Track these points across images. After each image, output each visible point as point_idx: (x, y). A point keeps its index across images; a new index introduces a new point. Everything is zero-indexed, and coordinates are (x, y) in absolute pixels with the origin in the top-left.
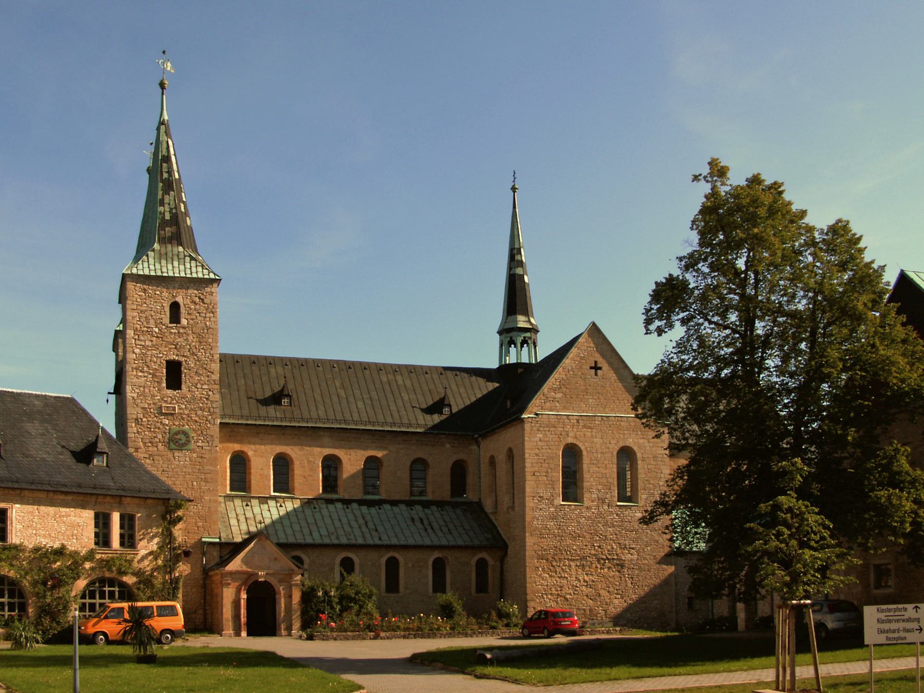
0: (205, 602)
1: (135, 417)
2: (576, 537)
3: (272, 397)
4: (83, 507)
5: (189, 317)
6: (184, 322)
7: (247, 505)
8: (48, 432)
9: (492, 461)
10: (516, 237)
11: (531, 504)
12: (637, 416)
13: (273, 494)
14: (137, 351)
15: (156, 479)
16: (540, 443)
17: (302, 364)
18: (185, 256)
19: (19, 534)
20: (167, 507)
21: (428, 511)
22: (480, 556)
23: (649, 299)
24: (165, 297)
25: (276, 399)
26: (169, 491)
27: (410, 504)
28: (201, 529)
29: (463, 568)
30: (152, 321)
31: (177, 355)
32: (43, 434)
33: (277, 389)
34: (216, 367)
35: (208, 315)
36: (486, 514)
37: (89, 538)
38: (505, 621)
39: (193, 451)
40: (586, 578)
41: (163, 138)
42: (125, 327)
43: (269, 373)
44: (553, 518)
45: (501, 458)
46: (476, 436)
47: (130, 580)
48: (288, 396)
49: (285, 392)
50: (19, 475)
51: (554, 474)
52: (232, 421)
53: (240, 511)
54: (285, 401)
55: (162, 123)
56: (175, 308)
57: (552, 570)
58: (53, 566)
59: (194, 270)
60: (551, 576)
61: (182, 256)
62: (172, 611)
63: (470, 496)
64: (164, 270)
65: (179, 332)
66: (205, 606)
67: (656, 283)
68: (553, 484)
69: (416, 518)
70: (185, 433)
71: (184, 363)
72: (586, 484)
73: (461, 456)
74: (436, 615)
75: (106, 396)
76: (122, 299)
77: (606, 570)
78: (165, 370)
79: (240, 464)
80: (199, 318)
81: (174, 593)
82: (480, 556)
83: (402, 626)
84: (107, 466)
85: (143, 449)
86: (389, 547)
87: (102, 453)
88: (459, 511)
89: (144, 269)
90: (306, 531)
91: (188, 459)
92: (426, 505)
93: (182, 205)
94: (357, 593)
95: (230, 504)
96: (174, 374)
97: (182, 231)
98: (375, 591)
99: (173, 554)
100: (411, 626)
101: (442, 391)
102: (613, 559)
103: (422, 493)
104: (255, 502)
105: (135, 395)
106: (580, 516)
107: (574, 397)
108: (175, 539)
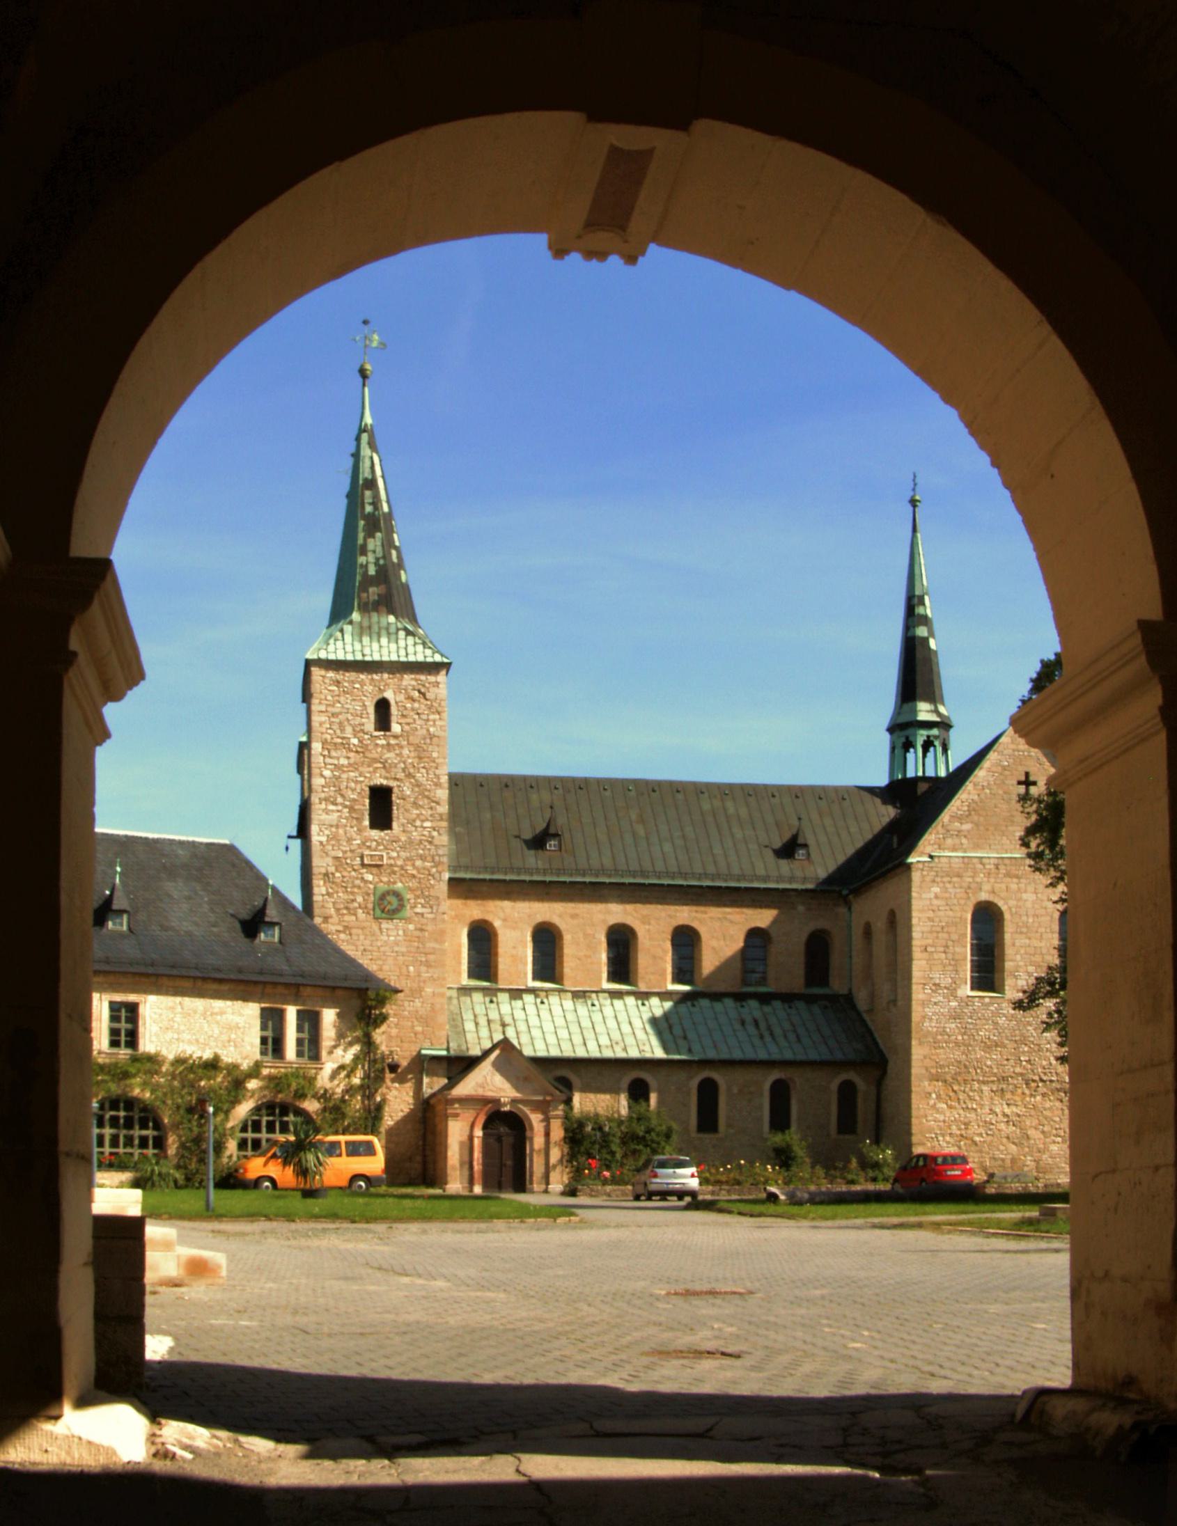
0: (424, 1145)
1: (323, 871)
2: (989, 1046)
3: (535, 842)
4: (245, 998)
5: (403, 721)
6: (396, 728)
7: (491, 1002)
8: (196, 894)
9: (868, 932)
10: (917, 578)
11: (921, 996)
12: (1029, 855)
13: (532, 984)
14: (327, 773)
15: (352, 961)
16: (935, 902)
17: (581, 786)
18: (398, 630)
19: (154, 1039)
20: (365, 1001)
21: (767, 1009)
22: (844, 1076)
23: (1029, 686)
24: (368, 688)
25: (538, 842)
26: (368, 976)
27: (740, 997)
28: (420, 1036)
29: (815, 1097)
30: (349, 730)
31: (386, 778)
32: (189, 898)
33: (541, 826)
34: (443, 794)
35: (432, 717)
36: (859, 1014)
37: (252, 1045)
38: (871, 1174)
39: (408, 920)
40: (1007, 1110)
41: (366, 451)
42: (309, 737)
43: (528, 802)
44: (955, 1016)
45: (880, 925)
46: (845, 892)
47: (311, 1106)
48: (556, 835)
49: (552, 831)
50: (154, 956)
51: (957, 949)
52: (468, 876)
53: (480, 1010)
54: (552, 844)
55: (362, 430)
56: (383, 708)
57: (952, 1097)
58: (204, 1083)
59: (411, 649)
60: (950, 1107)
61: (393, 629)
62: (369, 1150)
63: (837, 985)
64: (367, 651)
65: (388, 744)
66: (424, 1150)
67: (1042, 661)
68: (956, 964)
69: (748, 1019)
70: (397, 894)
71: (395, 790)
72: (1008, 965)
73: (821, 924)
74: (764, 1165)
75: (285, 841)
76: (307, 696)
77: (1039, 1098)
78: (367, 801)
79: (483, 941)
80: (418, 722)
81: (374, 1125)
82: (844, 1076)
83: (712, 1179)
84: (280, 942)
85: (335, 919)
86: (705, 1063)
87: (273, 924)
88: (816, 1009)
89: (346, 646)
90: (577, 1039)
91: (401, 932)
92: (765, 999)
93: (394, 553)
94: (648, 1131)
95: (466, 1000)
96: (381, 805)
97: (395, 592)
98: (675, 1126)
99: (378, 1069)
100: (724, 1178)
101: (796, 823)
102: (1051, 1081)
103: (763, 980)
104: (503, 997)
105: (324, 839)
106: (997, 1014)
107: (991, 828)
108: (377, 1048)
